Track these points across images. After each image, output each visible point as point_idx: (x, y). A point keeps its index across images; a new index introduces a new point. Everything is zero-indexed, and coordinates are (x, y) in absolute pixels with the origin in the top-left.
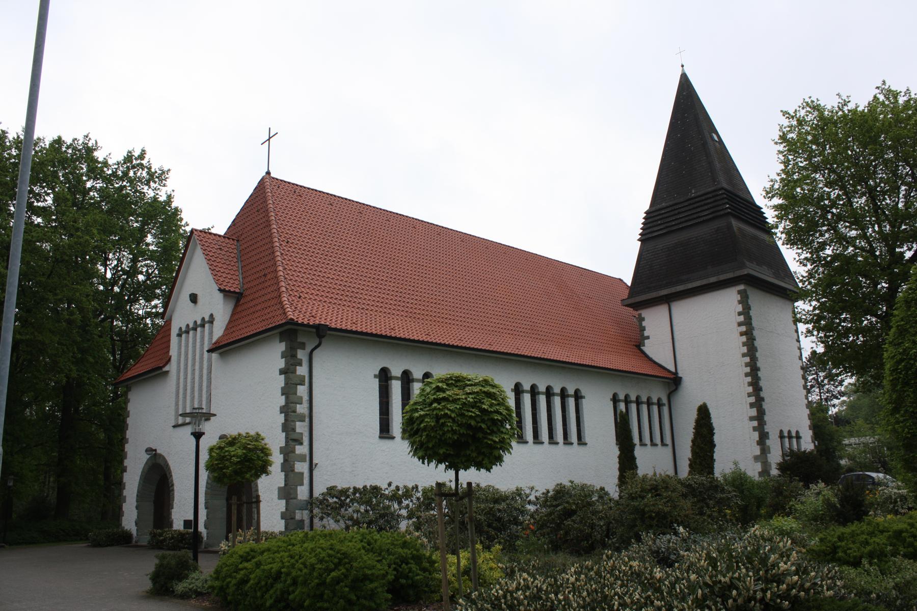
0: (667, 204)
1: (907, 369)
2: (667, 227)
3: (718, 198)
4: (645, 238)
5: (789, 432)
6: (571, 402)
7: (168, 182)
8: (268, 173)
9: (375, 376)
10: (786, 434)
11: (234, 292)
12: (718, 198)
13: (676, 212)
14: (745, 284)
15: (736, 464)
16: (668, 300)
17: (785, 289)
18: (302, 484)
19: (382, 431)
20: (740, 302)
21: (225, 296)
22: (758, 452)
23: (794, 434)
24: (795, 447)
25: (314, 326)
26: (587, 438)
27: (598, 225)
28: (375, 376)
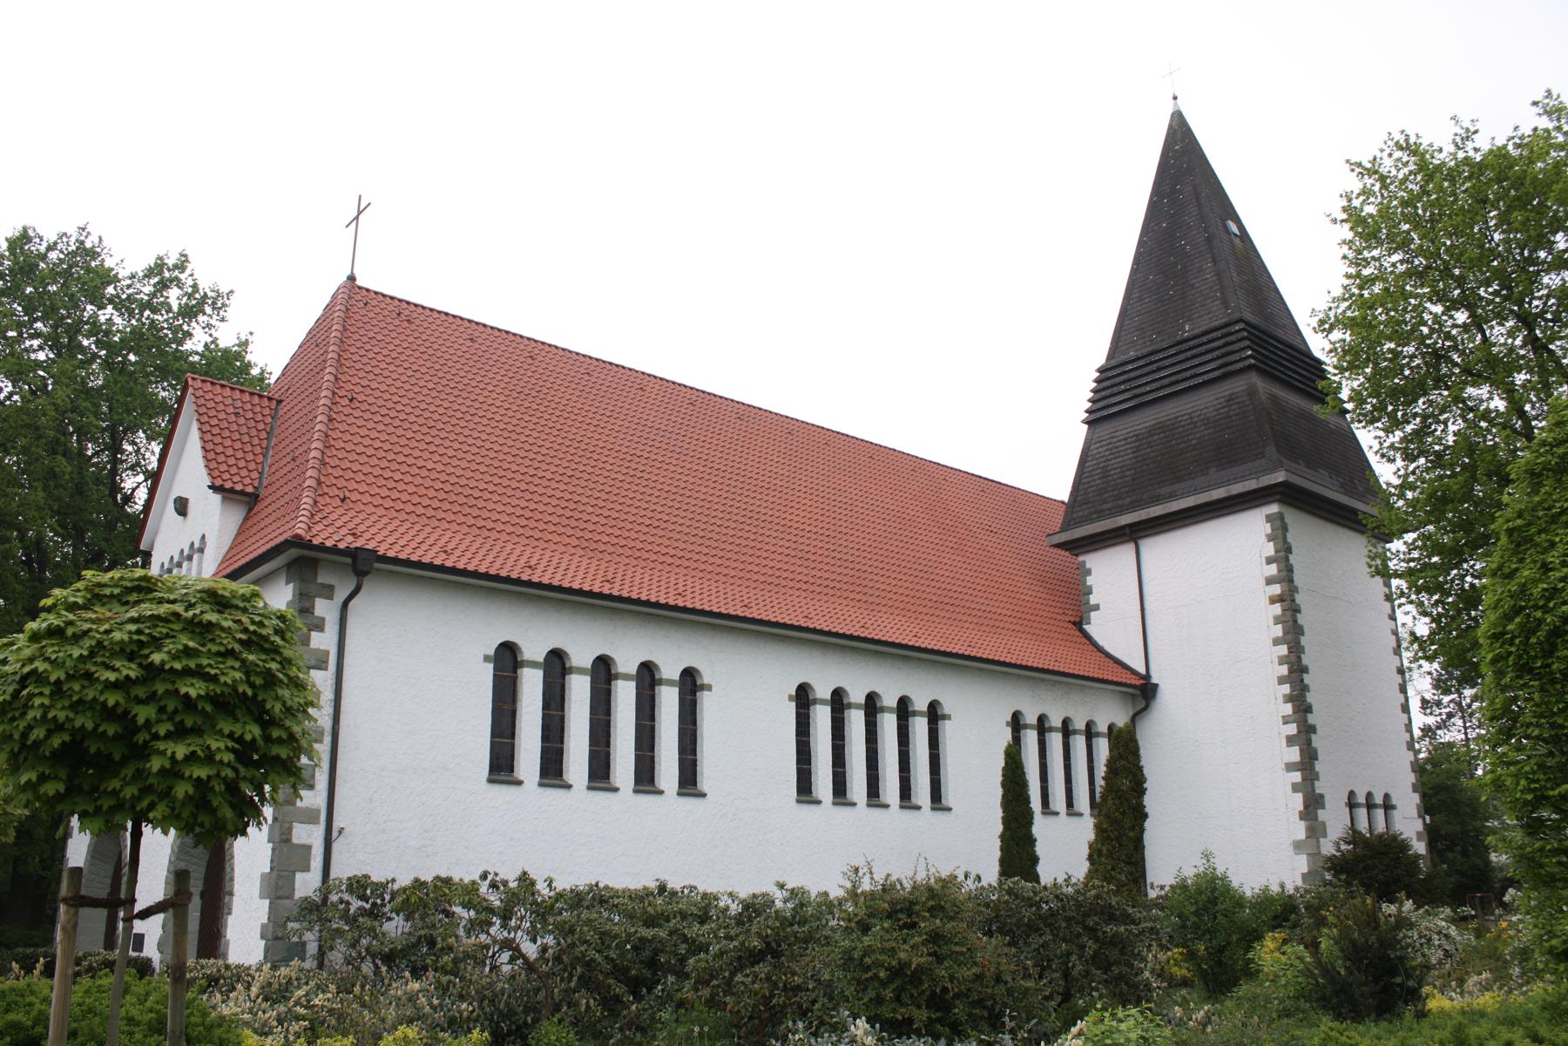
0: (1139, 353)
1: (1528, 630)
2: (1135, 396)
3: (1233, 338)
4: (1095, 419)
5: (1369, 795)
6: (920, 727)
7: (230, 314)
8: (352, 278)
9: (487, 659)
10: (1361, 799)
11: (242, 493)
12: (1233, 338)
13: (1154, 367)
14: (1280, 501)
15: (1207, 856)
16: (1134, 534)
17: (1354, 512)
18: (307, 869)
19: (869, 795)
20: (1270, 538)
21: (224, 499)
22: (1302, 835)
23: (1379, 800)
24: (1380, 826)
25: (347, 552)
26: (950, 795)
27: (1004, 389)
28: (487, 659)
